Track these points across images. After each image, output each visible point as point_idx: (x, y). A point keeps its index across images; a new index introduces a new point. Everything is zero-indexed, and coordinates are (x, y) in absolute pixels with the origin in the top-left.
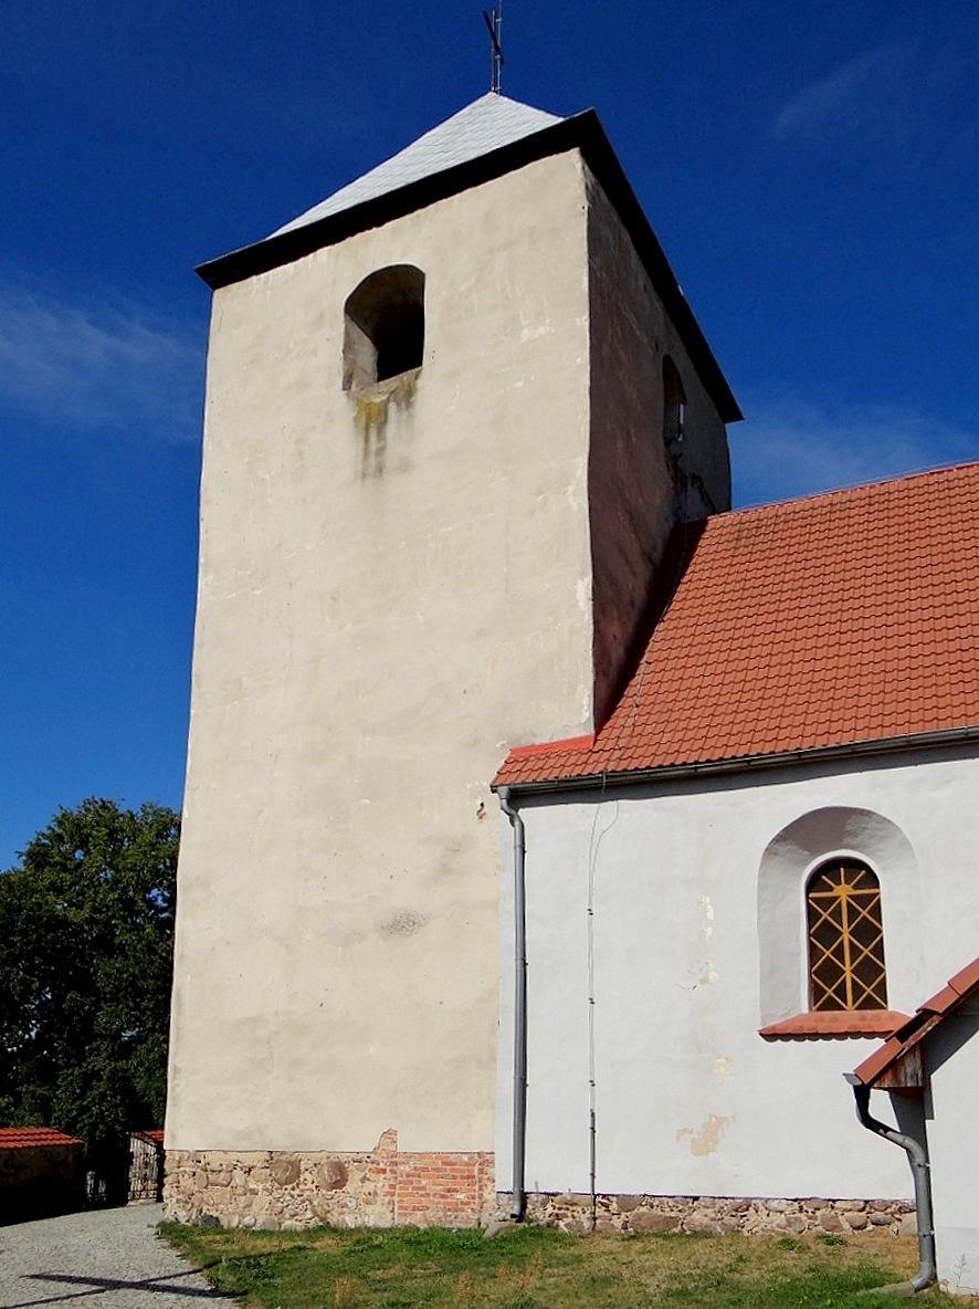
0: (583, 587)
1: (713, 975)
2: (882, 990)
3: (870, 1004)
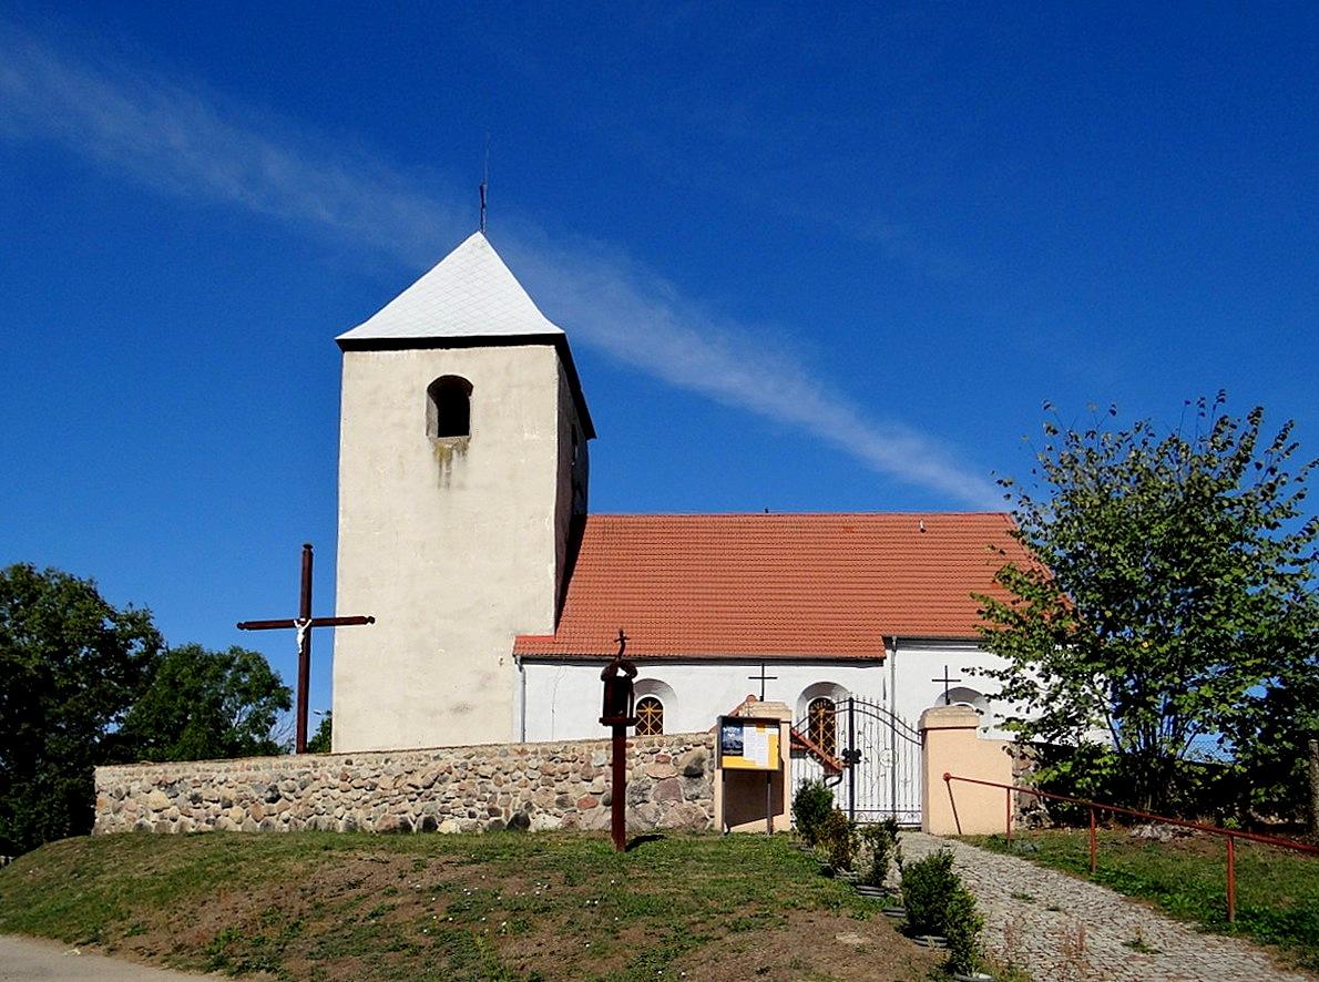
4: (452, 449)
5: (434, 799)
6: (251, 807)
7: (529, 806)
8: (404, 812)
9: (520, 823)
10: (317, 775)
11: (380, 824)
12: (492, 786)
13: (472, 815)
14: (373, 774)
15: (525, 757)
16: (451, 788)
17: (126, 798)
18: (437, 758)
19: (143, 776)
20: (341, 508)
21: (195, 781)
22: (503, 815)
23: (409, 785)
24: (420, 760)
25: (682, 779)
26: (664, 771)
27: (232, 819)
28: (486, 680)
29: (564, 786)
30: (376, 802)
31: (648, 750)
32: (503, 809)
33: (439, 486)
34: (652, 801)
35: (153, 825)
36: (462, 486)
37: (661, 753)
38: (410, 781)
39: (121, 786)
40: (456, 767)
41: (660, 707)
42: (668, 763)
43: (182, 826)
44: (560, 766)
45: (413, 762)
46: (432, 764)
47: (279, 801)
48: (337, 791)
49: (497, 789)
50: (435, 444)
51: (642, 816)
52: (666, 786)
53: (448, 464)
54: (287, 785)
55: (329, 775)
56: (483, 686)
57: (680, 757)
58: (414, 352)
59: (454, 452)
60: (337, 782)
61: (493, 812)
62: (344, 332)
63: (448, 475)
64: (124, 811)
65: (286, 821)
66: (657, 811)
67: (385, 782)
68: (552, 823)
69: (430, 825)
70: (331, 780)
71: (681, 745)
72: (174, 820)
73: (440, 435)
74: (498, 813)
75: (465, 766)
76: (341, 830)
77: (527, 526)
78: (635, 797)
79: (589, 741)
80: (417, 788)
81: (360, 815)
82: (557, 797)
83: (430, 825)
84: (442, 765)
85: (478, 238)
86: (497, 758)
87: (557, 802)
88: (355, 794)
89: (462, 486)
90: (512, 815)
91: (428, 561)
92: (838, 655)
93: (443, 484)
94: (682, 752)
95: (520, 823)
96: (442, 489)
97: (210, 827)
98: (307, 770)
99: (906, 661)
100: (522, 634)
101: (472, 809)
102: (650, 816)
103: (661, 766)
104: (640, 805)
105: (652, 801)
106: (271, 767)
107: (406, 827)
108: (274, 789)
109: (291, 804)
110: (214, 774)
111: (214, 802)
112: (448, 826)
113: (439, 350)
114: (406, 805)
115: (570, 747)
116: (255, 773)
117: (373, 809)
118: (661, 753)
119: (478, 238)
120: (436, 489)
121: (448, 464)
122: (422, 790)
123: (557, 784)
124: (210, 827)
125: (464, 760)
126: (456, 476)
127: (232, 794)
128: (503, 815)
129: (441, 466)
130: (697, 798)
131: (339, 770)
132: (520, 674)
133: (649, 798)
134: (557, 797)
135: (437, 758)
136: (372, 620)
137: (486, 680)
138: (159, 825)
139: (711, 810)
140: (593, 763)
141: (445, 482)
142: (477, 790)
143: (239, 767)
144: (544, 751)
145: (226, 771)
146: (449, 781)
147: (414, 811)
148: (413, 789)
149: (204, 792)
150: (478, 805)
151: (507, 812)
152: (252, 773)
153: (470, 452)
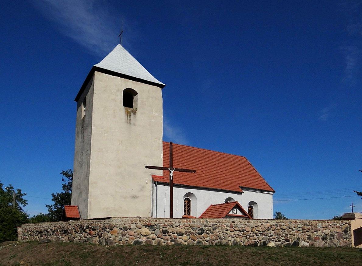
0: (162, 155)
1: (178, 210)
2: (189, 213)
3: (188, 215)
4: (131, 112)
5: (266, 235)
6: (191, 236)
7: (299, 239)
8: (256, 239)
9: (296, 244)
10: (220, 225)
11: (246, 243)
12: (286, 232)
13: (280, 241)
14: (243, 226)
15: (297, 224)
16: (272, 232)
17: (128, 230)
18: (267, 222)
19: (138, 222)
20: (93, 123)
21: (165, 225)
22: (290, 241)
23: (257, 231)
24: (261, 223)
25: (343, 233)
26: (339, 230)
27: (184, 240)
28: (142, 189)
29: (309, 233)
30: (244, 236)
31: (334, 224)
32: (290, 239)
33: (127, 123)
34: (336, 239)
35: (144, 242)
36: (134, 125)
37: (337, 225)
38: (257, 229)
39: (127, 225)
40: (273, 226)
41: (190, 201)
42: (340, 228)
43: (159, 243)
44: (308, 227)
45: (258, 223)
46: (265, 224)
47: (203, 234)
48: (229, 231)
49: (288, 233)
50: (126, 109)
51: (333, 243)
52: (339, 234)
53: (130, 116)
54: (208, 228)
55: (225, 226)
56: (141, 190)
57: (342, 226)
58: (119, 78)
59: (132, 113)
60: (229, 228)
61: (287, 240)
62: (96, 64)
63: (130, 120)
64: (127, 235)
65: (207, 241)
66: (337, 242)
67: (249, 229)
68: (307, 244)
69: (265, 244)
70: (226, 227)
71: (342, 223)
72: (154, 239)
73: (75, 101)
74: (289, 241)
75: (277, 225)
76: (230, 245)
77: (155, 141)
78: (331, 238)
79: (316, 220)
80: (260, 231)
81: (238, 240)
82: (307, 236)
83: (265, 244)
84: (268, 225)
85: (119, 46)
86: (288, 224)
87: (308, 238)
88: (236, 233)
89: (134, 125)
90: (294, 241)
91: (123, 147)
92: (226, 189)
93: (128, 122)
94: (342, 225)
95: (296, 244)
96: (128, 124)
97: (173, 243)
98: (217, 223)
99: (245, 193)
100: (153, 175)
101: (280, 239)
102: (336, 243)
103: (338, 229)
104: (333, 240)
105: (336, 239)
106: (200, 222)
107: (255, 245)
108: (202, 230)
109: (209, 235)
110: (174, 223)
111: (173, 233)
112: (272, 244)
113: (127, 79)
114: (256, 237)
115: (311, 222)
116: (193, 224)
117: (243, 238)
118: (337, 225)
119: (119, 46)
120: (126, 123)
121: (130, 116)
122: (261, 232)
123: (307, 233)
124: (173, 243)
125: (276, 224)
126: (132, 121)
127: (183, 231)
128: (290, 241)
129: (127, 117)
130: (347, 238)
131: (229, 224)
132: (156, 187)
133: (335, 238)
134: (307, 236)
135: (267, 222)
136: (147, 167)
137: (142, 189)
138: (146, 241)
139: (351, 242)
140: (317, 227)
141: (129, 122)
142: (281, 233)
143: (185, 221)
144: (303, 222)
145: (179, 222)
146: (271, 230)
147: (260, 239)
148: (258, 232)
149: (170, 229)
150: (282, 238)
151: (292, 241)
152: (192, 223)
153: (137, 114)
